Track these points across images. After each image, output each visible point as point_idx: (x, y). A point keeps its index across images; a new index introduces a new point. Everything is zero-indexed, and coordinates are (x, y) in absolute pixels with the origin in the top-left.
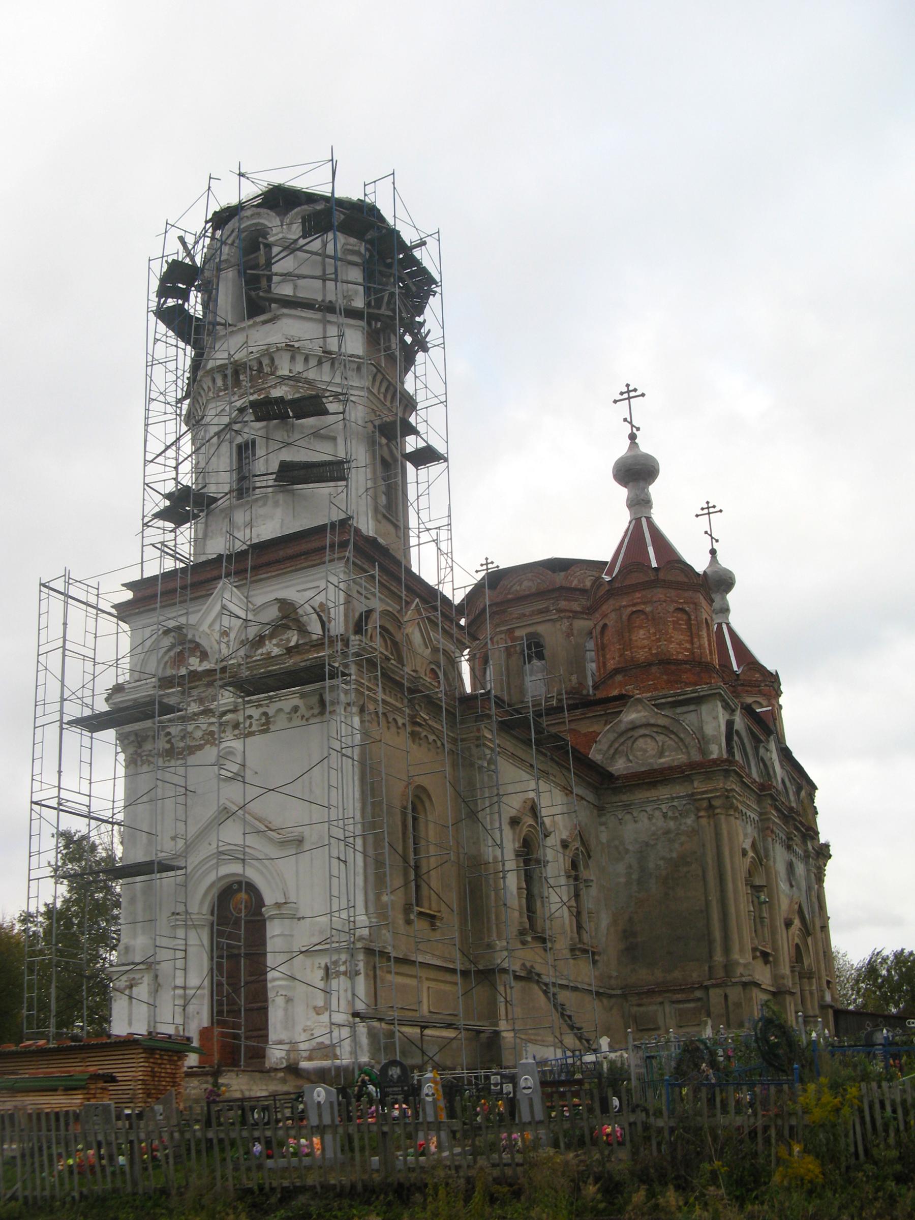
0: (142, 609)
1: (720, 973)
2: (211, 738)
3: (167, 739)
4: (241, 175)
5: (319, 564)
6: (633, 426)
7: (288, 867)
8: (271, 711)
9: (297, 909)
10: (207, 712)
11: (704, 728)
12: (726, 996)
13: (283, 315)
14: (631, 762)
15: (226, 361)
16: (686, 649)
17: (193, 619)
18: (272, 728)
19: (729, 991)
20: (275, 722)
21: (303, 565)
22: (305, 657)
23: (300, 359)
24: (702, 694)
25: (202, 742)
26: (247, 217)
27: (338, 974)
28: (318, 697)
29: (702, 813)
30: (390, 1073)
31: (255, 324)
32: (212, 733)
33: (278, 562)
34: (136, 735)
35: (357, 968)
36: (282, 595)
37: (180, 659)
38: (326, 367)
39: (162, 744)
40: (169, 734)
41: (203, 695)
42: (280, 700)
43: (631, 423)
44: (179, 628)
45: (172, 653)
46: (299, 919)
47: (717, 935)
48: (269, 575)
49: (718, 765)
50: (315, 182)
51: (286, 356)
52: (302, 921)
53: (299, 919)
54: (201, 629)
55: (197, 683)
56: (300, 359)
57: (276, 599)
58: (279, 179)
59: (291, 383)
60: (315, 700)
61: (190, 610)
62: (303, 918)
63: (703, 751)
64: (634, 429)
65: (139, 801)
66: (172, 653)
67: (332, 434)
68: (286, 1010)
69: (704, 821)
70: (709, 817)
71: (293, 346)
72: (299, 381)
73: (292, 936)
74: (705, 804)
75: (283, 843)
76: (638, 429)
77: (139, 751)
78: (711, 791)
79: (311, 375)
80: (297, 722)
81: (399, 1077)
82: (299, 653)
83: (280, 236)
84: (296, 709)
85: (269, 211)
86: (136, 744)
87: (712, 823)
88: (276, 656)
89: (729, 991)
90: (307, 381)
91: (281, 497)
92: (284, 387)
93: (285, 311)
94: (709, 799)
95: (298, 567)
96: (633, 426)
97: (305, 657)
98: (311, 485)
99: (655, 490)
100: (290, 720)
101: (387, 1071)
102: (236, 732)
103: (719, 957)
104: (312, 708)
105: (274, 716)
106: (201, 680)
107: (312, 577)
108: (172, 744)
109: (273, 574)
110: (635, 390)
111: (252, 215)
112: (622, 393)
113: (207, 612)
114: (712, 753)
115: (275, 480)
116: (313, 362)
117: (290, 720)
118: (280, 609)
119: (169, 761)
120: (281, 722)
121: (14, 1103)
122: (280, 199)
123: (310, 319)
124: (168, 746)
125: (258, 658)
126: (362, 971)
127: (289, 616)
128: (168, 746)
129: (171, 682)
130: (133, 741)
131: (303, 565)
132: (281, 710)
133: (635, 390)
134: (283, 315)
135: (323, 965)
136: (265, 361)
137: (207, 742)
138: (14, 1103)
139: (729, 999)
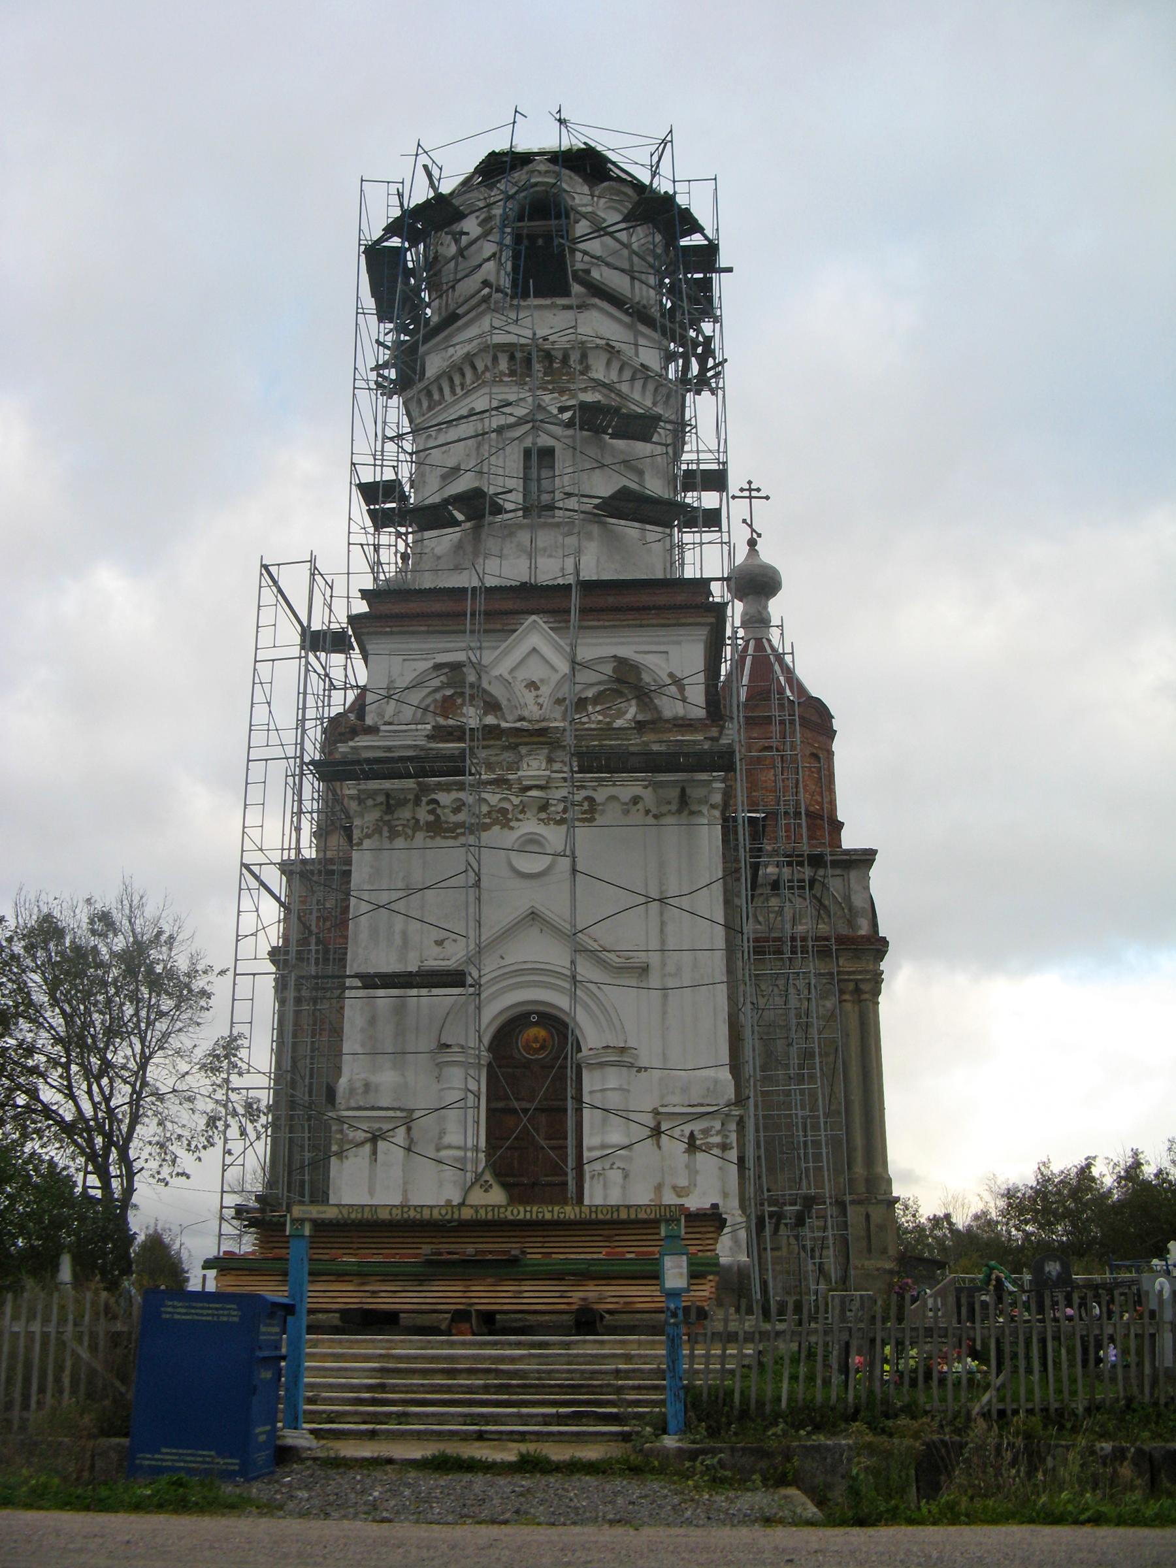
0: (394, 629)
1: (861, 1188)
2: (502, 818)
3: (431, 807)
4: (561, 121)
5: (674, 625)
6: (753, 531)
7: (624, 1000)
8: (600, 795)
9: (636, 1057)
10: (500, 782)
11: (853, 897)
12: (868, 1216)
13: (594, 306)
14: (760, 923)
15: (529, 341)
16: (818, 803)
17: (487, 657)
18: (592, 819)
19: (871, 1209)
20: (603, 811)
21: (651, 622)
22: (665, 737)
23: (616, 365)
24: (854, 857)
25: (488, 821)
26: (539, 172)
27: (707, 1149)
28: (678, 790)
29: (847, 997)
30: (1047, 1269)
31: (553, 306)
32: (504, 812)
33: (617, 609)
34: (388, 796)
35: (728, 1141)
36: (624, 652)
37: (447, 706)
38: (638, 384)
39: (423, 815)
40: (435, 802)
41: (493, 759)
42: (614, 785)
43: (750, 526)
44: (456, 667)
45: (438, 696)
46: (639, 1070)
47: (859, 1141)
48: (601, 623)
49: (872, 944)
50: (632, 160)
51: (604, 357)
52: (643, 1074)
53: (639, 1070)
54: (496, 672)
55: (492, 742)
56: (616, 365)
57: (615, 656)
58: (603, 142)
59: (605, 391)
60: (674, 793)
61: (485, 644)
62: (646, 1069)
63: (851, 923)
64: (755, 536)
65: (439, 885)
66: (438, 696)
67: (640, 466)
68: (624, 1187)
69: (848, 1006)
70: (853, 1002)
71: (613, 347)
72: (611, 391)
73: (628, 1091)
74: (851, 986)
75: (621, 970)
76: (759, 535)
77: (387, 818)
78: (860, 972)
79: (624, 388)
80: (637, 817)
81: (1059, 1275)
82: (654, 730)
83: (590, 209)
84: (636, 800)
85: (573, 175)
86: (384, 807)
87: (856, 1009)
88: (619, 729)
89: (871, 1209)
90: (619, 394)
91: (595, 529)
92: (597, 394)
93: (596, 301)
94: (857, 982)
95: (644, 622)
96: (753, 531)
97: (665, 737)
98: (623, 522)
99: (776, 607)
100: (626, 812)
101: (1043, 1268)
102: (543, 815)
103: (859, 1170)
104: (669, 803)
105: (603, 804)
106: (500, 739)
107: (656, 639)
108: (438, 816)
109: (607, 624)
110: (758, 490)
111: (547, 172)
112: (742, 490)
113: (506, 653)
114: (860, 928)
115: (596, 507)
116: (627, 375)
117: (626, 812)
118: (615, 670)
119: (432, 838)
120: (610, 815)
121: (581, 1294)
122: (588, 163)
123: (619, 321)
124: (431, 818)
125: (593, 726)
126: (735, 1144)
127: (627, 680)
128: (431, 818)
129: (451, 734)
130: (382, 803)
131: (651, 622)
132: (613, 798)
133: (758, 490)
134: (594, 306)
135: (687, 1133)
136: (574, 357)
137: (496, 822)
138: (581, 1294)
139: (872, 1219)
